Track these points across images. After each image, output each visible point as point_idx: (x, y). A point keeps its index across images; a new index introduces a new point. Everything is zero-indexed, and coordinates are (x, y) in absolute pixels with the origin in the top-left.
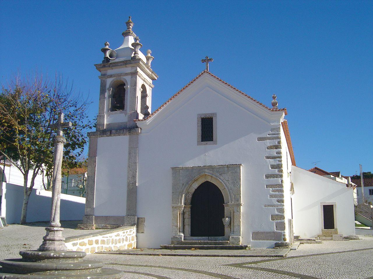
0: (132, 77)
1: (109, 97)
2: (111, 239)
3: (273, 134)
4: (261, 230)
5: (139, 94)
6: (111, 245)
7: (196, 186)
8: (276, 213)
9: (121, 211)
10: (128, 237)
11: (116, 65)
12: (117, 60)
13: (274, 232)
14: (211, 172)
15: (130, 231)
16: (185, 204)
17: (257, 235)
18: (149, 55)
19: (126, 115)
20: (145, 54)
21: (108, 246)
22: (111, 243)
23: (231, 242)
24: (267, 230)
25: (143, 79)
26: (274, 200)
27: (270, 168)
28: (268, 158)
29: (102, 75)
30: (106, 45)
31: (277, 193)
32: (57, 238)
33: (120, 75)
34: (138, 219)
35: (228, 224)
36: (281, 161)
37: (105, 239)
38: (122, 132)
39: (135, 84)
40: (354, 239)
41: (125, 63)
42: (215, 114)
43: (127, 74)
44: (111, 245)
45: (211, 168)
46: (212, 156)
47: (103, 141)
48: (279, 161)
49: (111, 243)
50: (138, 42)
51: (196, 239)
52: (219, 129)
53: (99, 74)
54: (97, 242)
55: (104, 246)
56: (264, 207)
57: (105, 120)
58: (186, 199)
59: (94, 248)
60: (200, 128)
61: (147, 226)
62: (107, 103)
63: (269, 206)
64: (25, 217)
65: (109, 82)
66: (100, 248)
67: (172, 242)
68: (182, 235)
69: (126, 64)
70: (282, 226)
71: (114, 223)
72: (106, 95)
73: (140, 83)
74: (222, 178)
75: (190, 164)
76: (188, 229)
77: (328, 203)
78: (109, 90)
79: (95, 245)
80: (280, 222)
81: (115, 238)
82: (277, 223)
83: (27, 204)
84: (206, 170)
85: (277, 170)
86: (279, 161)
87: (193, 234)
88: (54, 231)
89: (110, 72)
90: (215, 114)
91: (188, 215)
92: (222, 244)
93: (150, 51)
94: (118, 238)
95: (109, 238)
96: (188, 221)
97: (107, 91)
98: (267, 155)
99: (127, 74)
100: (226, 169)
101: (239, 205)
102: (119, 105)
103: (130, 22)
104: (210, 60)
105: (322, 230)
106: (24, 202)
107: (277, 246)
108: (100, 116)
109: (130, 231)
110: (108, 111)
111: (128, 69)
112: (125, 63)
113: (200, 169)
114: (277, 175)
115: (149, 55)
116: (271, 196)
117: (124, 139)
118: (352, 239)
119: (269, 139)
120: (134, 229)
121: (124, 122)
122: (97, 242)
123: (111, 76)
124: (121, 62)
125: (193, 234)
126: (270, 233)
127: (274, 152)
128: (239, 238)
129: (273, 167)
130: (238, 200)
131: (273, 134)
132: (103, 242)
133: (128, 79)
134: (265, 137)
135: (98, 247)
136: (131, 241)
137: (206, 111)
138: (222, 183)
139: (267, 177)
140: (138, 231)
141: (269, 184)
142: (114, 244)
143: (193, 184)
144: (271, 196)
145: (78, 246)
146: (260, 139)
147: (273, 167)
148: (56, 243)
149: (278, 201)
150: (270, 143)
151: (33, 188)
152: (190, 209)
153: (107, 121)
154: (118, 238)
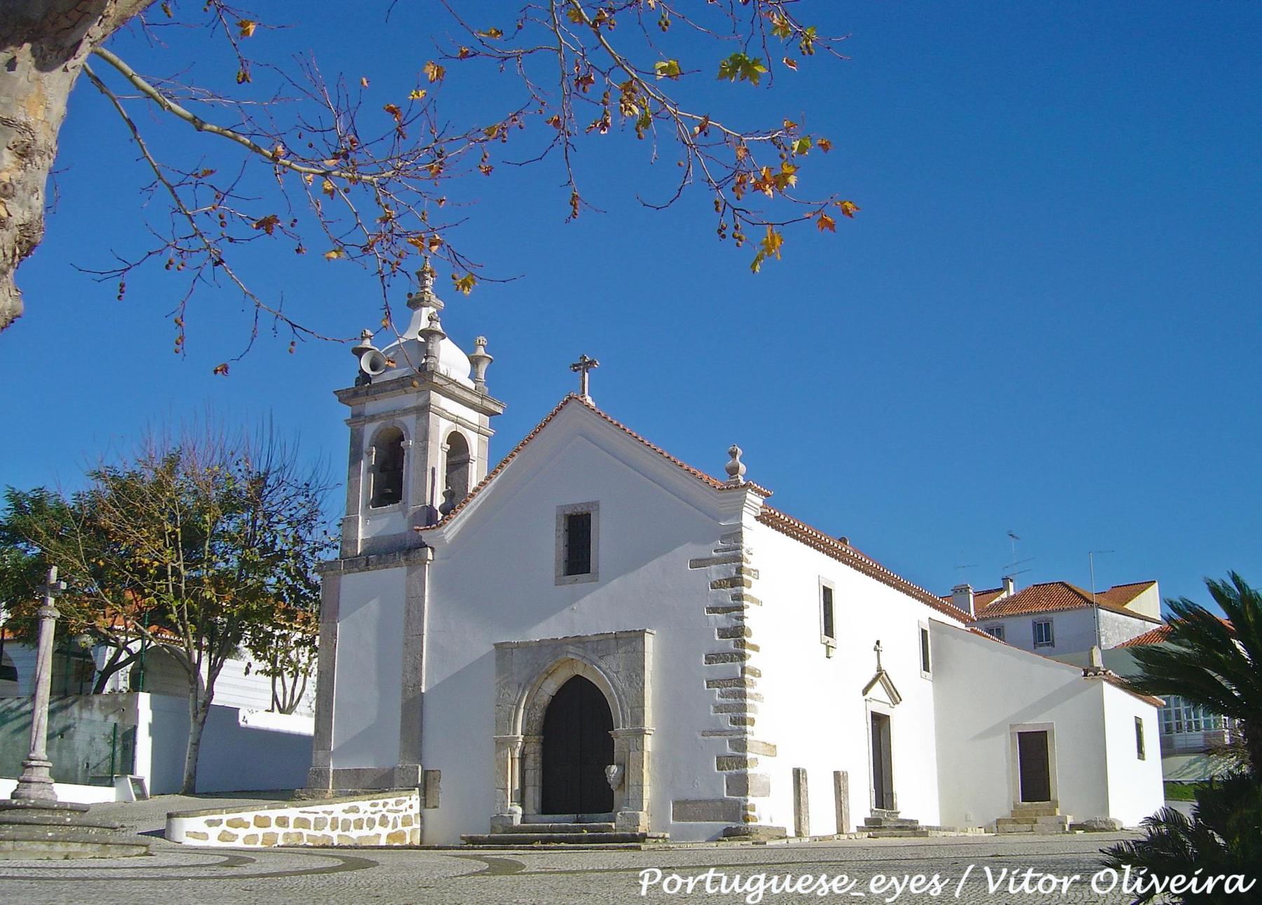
0: (418, 419)
1: (369, 470)
2: (329, 818)
3: (726, 550)
4: (693, 796)
5: (438, 459)
6: (327, 831)
7: (551, 687)
8: (729, 751)
9: (390, 755)
10: (391, 816)
11: (384, 388)
12: (388, 376)
13: (723, 801)
14: (581, 652)
15: (397, 803)
16: (525, 734)
17: (685, 809)
18: (481, 351)
19: (405, 513)
20: (466, 345)
21: (319, 833)
22: (328, 827)
23: (617, 825)
24: (707, 794)
25: (449, 416)
26: (725, 720)
27: (717, 638)
28: (713, 610)
29: (353, 416)
30: (363, 338)
31: (731, 700)
32: (34, 779)
33: (392, 414)
34: (425, 773)
35: (619, 781)
36: (742, 618)
37: (311, 818)
38: (390, 558)
39: (424, 437)
40: (1102, 830)
41: (402, 384)
42: (596, 504)
43: (406, 412)
44: (327, 831)
45: (579, 641)
46: (588, 612)
47: (351, 583)
48: (737, 618)
49: (328, 827)
50: (438, 327)
51: (550, 821)
52: (605, 543)
53: (347, 411)
54: (282, 822)
55: (305, 832)
56: (700, 737)
57: (360, 530)
58: (527, 722)
59: (275, 835)
60: (562, 542)
61: (445, 790)
62: (366, 484)
63: (712, 733)
64: (192, 776)
65: (370, 430)
66: (294, 836)
67: (493, 827)
68: (519, 810)
69: (403, 386)
70: (740, 784)
71: (381, 784)
72: (363, 465)
73: (441, 429)
74: (603, 666)
75: (537, 634)
76: (533, 795)
77: (1033, 724)
78: (370, 454)
79: (274, 828)
80: (737, 775)
81: (342, 816)
82: (729, 777)
83: (196, 744)
84: (571, 648)
85: (731, 641)
86: (737, 618)
87: (547, 808)
88: (31, 766)
89: (371, 407)
90: (596, 504)
91: (533, 762)
92: (600, 829)
93: (482, 340)
94: (352, 817)
95: (321, 815)
96: (534, 776)
97: (365, 456)
98: (711, 604)
99: (406, 412)
100: (613, 643)
101: (641, 733)
102: (390, 491)
103: (425, 272)
104: (592, 363)
105: (1015, 806)
106: (190, 740)
107: (729, 834)
108: (348, 523)
109: (397, 803)
110: (367, 506)
111: (410, 399)
112: (402, 384)
113: (555, 646)
114: (732, 654)
115: (481, 351)
116: (719, 709)
117: (394, 576)
118: (1094, 830)
119: (716, 561)
120: (414, 799)
121: (400, 534)
122: (282, 822)
123: (372, 418)
124: (391, 381)
125: (547, 808)
126: (713, 801)
127: (726, 597)
128: (637, 817)
129: (724, 633)
130: (639, 719)
131: (726, 550)
132: (303, 823)
133: (409, 421)
134: (708, 556)
135: (287, 835)
136: (400, 827)
137: (576, 498)
138: (605, 675)
139: (710, 659)
140: (424, 804)
141: (714, 677)
142: (339, 831)
143: (546, 684)
144: (719, 709)
145: (224, 826)
146: (697, 563)
147: (724, 633)
148: (33, 785)
149: (734, 722)
150: (718, 572)
151: (213, 702)
152: (538, 747)
153: (365, 533)
154: (352, 817)
